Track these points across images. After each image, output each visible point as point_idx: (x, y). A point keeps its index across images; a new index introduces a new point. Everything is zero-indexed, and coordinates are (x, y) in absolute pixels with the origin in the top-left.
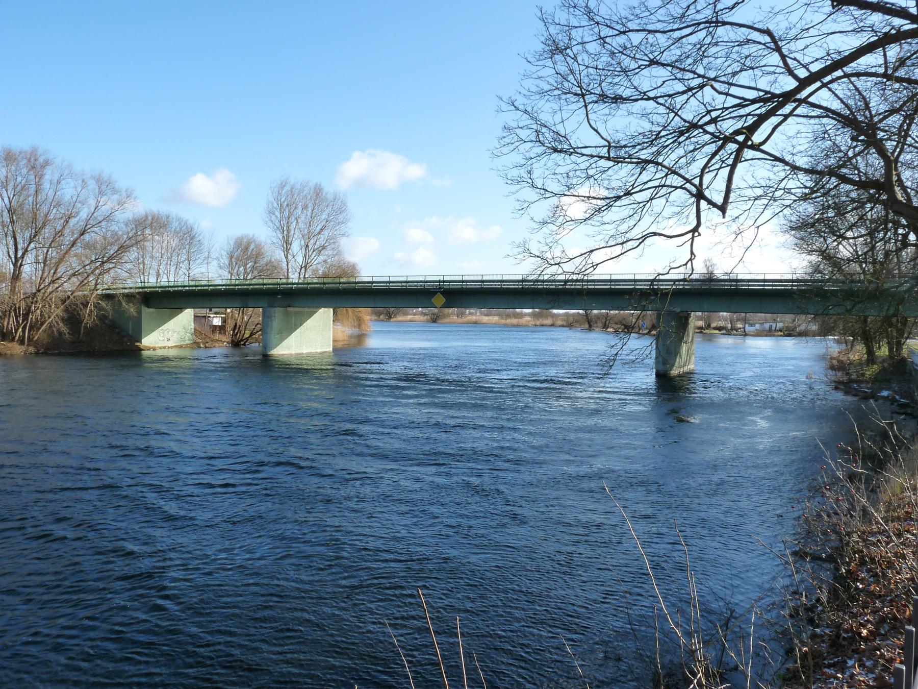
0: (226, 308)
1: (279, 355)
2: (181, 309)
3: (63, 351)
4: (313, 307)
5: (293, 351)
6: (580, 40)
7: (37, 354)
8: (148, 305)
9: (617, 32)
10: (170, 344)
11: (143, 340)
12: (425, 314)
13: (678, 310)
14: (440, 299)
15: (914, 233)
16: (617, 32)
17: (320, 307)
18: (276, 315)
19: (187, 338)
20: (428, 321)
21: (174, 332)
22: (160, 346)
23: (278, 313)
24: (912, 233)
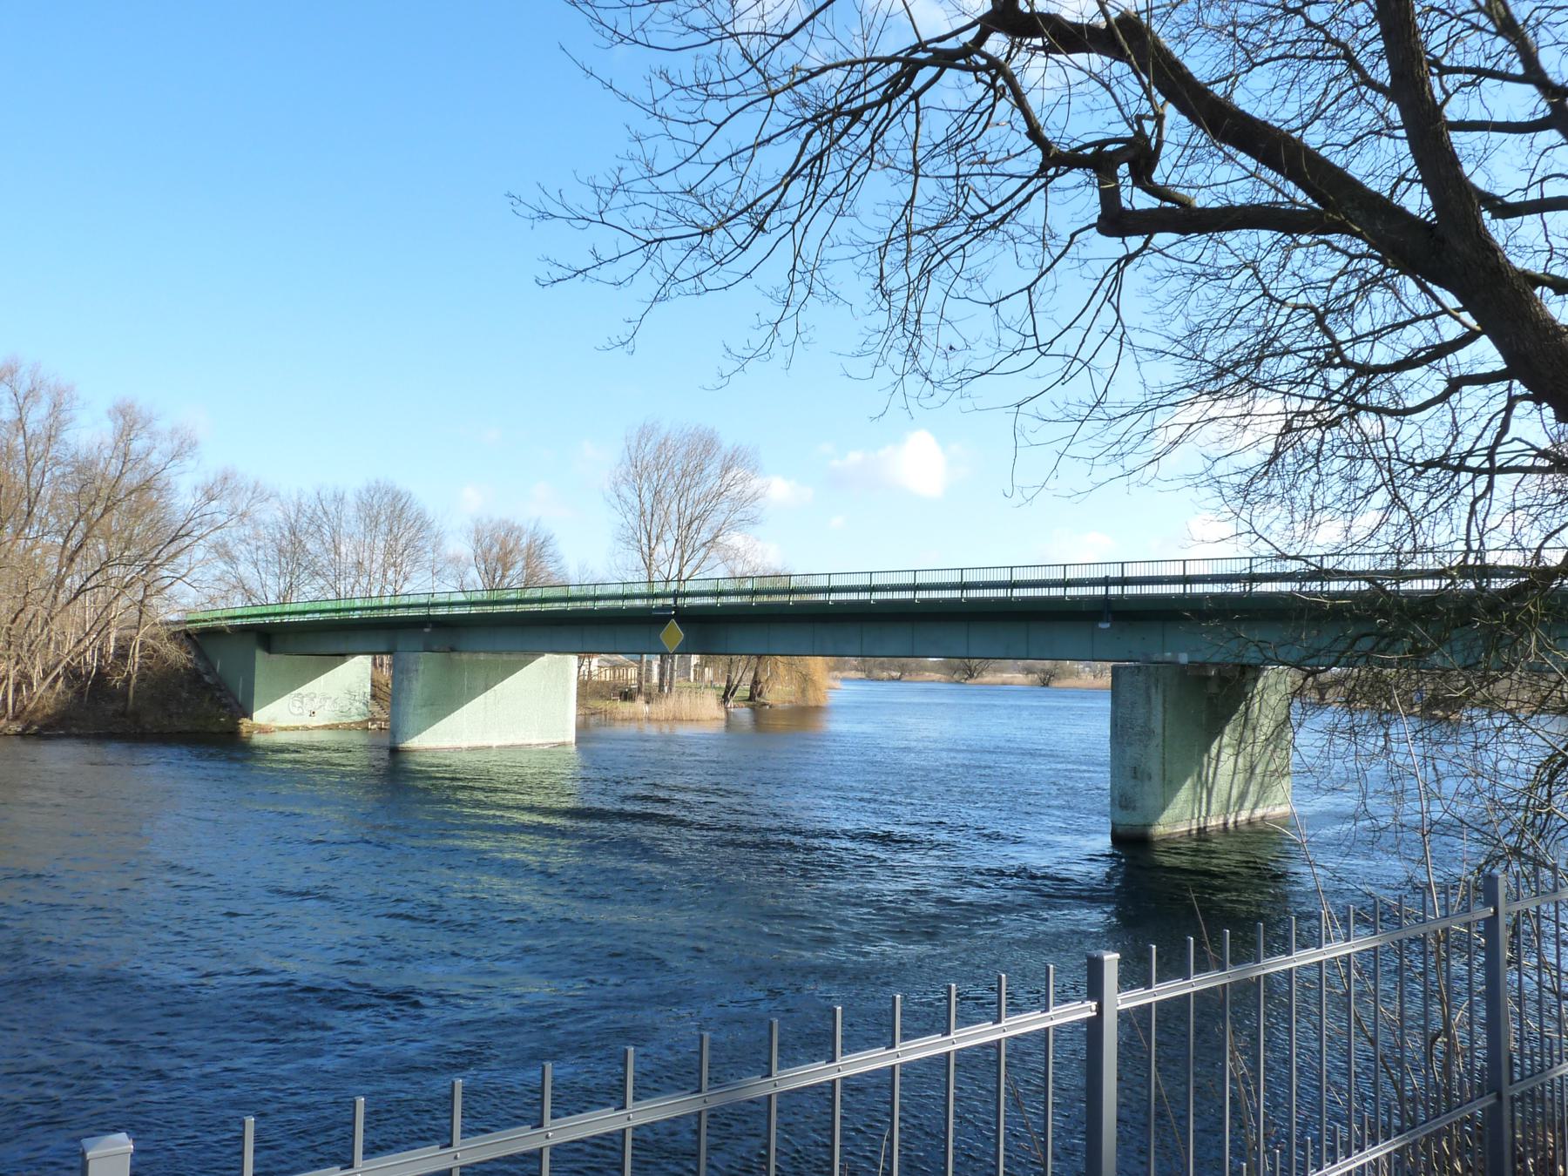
0: (642, 654)
1: (435, 750)
2: (343, 656)
3: (74, 730)
4: (523, 651)
5: (446, 743)
6: (926, 168)
7: (21, 735)
8: (269, 649)
9: (776, 40)
10: (314, 722)
11: (255, 715)
12: (1029, 671)
13: (1184, 658)
14: (674, 634)
15: (1550, 405)
16: (776, 40)
17: (541, 653)
18: (421, 668)
19: (354, 711)
20: (1033, 684)
21: (325, 699)
22: (279, 724)
23: (425, 667)
24: (983, 48)
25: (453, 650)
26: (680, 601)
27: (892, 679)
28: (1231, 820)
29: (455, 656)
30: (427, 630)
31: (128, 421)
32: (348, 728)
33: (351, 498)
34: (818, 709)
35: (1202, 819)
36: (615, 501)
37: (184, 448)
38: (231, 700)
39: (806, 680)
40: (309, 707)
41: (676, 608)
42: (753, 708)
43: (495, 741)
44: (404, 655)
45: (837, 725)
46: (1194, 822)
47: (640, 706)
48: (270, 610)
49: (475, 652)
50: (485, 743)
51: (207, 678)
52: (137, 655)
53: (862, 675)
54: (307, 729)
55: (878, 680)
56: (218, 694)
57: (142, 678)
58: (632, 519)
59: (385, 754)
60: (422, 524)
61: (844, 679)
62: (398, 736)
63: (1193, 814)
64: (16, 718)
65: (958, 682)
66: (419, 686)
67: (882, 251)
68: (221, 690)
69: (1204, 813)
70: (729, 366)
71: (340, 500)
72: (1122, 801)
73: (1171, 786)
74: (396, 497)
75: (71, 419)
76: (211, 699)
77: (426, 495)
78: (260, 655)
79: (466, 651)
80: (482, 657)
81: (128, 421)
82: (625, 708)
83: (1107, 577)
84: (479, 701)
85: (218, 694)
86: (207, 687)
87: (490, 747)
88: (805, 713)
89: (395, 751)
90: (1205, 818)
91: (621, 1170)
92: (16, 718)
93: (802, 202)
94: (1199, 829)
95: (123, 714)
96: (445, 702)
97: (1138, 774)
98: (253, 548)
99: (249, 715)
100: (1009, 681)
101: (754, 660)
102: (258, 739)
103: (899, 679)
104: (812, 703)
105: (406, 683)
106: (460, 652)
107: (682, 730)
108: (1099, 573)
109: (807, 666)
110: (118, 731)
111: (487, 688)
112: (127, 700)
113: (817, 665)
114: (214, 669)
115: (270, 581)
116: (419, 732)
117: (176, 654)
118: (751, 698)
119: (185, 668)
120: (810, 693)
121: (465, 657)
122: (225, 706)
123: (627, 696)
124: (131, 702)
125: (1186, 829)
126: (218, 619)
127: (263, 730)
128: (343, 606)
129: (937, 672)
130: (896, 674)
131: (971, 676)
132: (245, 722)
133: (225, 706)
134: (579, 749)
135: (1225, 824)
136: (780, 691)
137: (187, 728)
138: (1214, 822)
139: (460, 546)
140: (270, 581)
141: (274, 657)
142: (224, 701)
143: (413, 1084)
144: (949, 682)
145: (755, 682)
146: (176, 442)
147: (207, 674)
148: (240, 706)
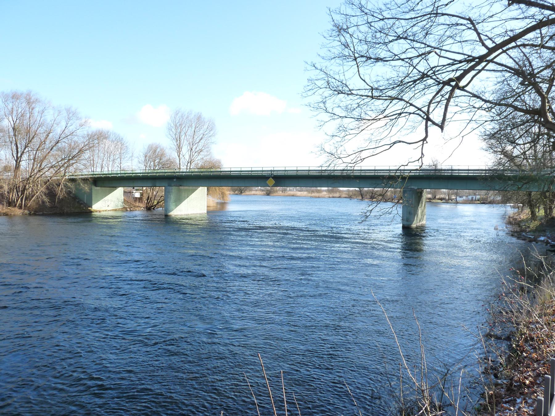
0: (143, 187)
2: (116, 187)
13: (416, 188)
14: (271, 182)
17: (199, 186)
19: (119, 205)
23: (174, 189)
29: (181, 188)
30: (175, 180)
43: (195, 213)
59: (164, 217)
65: (237, 194)
66: (172, 197)
67: (382, 77)
81: (71, 114)
84: (186, 201)
93: (483, 69)
96: (179, 201)
111: (188, 197)
143: (197, 316)
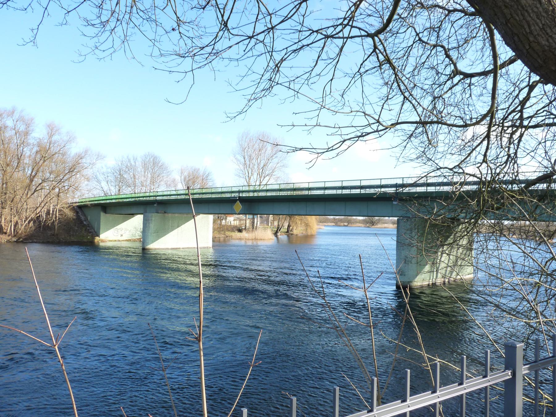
2: (133, 215)
3: (35, 240)
7: (17, 242)
8: (105, 212)
11: (101, 236)
14: (238, 206)
18: (153, 219)
19: (137, 235)
23: (155, 218)
25: (165, 213)
26: (241, 195)
27: (345, 226)
28: (447, 280)
29: (166, 215)
30: (155, 205)
31: (52, 129)
32: (134, 241)
33: (139, 160)
34: (312, 236)
35: (434, 280)
36: (235, 161)
37: (71, 139)
38: (92, 230)
39: (307, 225)
40: (120, 233)
41: (239, 197)
42: (288, 236)
44: (150, 215)
45: (320, 241)
46: (431, 281)
47: (244, 234)
48: (112, 197)
49: (174, 213)
50: (178, 247)
51: (85, 223)
52: (57, 214)
53: (333, 224)
54: (119, 241)
55: (339, 226)
56: (88, 228)
57: (60, 222)
58: (242, 167)
60: (162, 167)
61: (325, 226)
62: (145, 244)
63: (430, 278)
64: (15, 236)
65: (368, 227)
66: (152, 226)
68: (89, 227)
69: (435, 277)
70: (21, 42)
71: (135, 160)
72: (401, 272)
73: (420, 265)
74: (155, 158)
75: (33, 130)
76: (85, 230)
77: (165, 158)
78: (102, 214)
79: (170, 213)
80: (176, 215)
81: (52, 129)
82: (238, 234)
83: (396, 184)
85: (88, 228)
86: (84, 226)
87: (179, 248)
88: (307, 238)
89: (144, 249)
90: (436, 279)
91: (203, 415)
92: (15, 236)
94: (433, 284)
95: (53, 235)
96: (163, 231)
97: (407, 261)
98: (106, 176)
99: (98, 236)
100: (387, 227)
101: (288, 218)
102: (102, 244)
103: (347, 226)
104: (309, 234)
105: (148, 224)
106: (168, 213)
107: (260, 243)
108: (393, 182)
109: (307, 220)
110: (51, 241)
111: (178, 227)
112: (55, 230)
113: (313, 220)
114: (88, 219)
115: (112, 188)
116: (153, 242)
117: (70, 214)
118: (287, 232)
119: (74, 219)
120: (309, 230)
121: (170, 215)
122: (90, 232)
123: (240, 231)
124: (56, 231)
125: (427, 283)
126: (86, 202)
127: (103, 241)
128: (137, 196)
129: (361, 223)
130: (346, 224)
131: (373, 225)
132: (97, 238)
133: (90, 232)
134: (214, 249)
135: (444, 282)
136: (298, 230)
137: (75, 240)
138: (439, 281)
139: (177, 176)
140: (112, 188)
141: (108, 215)
142: (90, 231)
144: (365, 227)
145: (289, 226)
146: (69, 137)
147: (85, 221)
148: (96, 232)
